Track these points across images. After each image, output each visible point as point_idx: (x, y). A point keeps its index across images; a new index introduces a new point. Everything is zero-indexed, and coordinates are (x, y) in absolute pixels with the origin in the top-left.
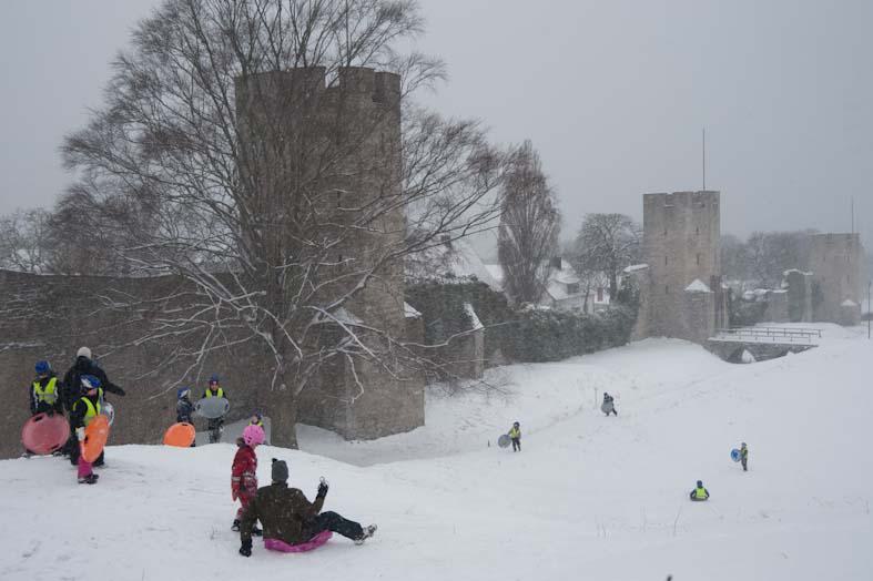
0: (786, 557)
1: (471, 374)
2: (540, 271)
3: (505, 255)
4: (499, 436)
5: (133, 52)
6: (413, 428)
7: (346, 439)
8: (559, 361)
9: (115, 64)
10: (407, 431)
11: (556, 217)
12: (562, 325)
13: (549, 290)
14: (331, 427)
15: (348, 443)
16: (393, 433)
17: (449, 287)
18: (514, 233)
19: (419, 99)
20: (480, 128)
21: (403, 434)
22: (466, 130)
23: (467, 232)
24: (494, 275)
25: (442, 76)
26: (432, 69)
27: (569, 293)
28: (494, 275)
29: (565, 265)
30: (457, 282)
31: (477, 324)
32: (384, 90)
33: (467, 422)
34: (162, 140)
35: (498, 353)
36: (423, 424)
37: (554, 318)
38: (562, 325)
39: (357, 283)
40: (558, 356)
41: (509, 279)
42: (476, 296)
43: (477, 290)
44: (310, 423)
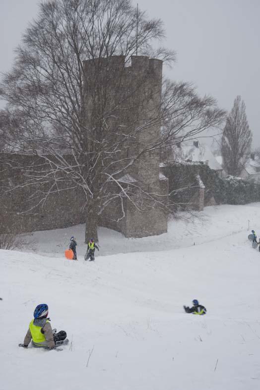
0: (173, 358)
1: (197, 208)
2: (241, 160)
3: (224, 152)
4: (248, 235)
5: (24, 46)
6: (162, 233)
7: (126, 237)
8: (244, 204)
9: (16, 51)
10: (158, 235)
11: (251, 134)
12: (246, 187)
13: (247, 169)
14: (120, 231)
15: (127, 239)
16: (150, 235)
17: (188, 167)
18: (229, 141)
19: (170, 74)
20: (192, 87)
21: (156, 236)
22: (185, 87)
23: (184, 140)
24: (216, 162)
25: (173, 60)
26: (170, 56)
27: (257, 171)
28: (216, 162)
29: (256, 158)
30: (192, 164)
31: (201, 184)
32: (150, 69)
33: (189, 232)
34: (37, 89)
35: (213, 199)
36: (166, 232)
37: (242, 183)
38: (246, 187)
39: (129, 162)
40: (246, 202)
41: (225, 165)
42: (202, 171)
43: (203, 169)
44: (111, 228)
